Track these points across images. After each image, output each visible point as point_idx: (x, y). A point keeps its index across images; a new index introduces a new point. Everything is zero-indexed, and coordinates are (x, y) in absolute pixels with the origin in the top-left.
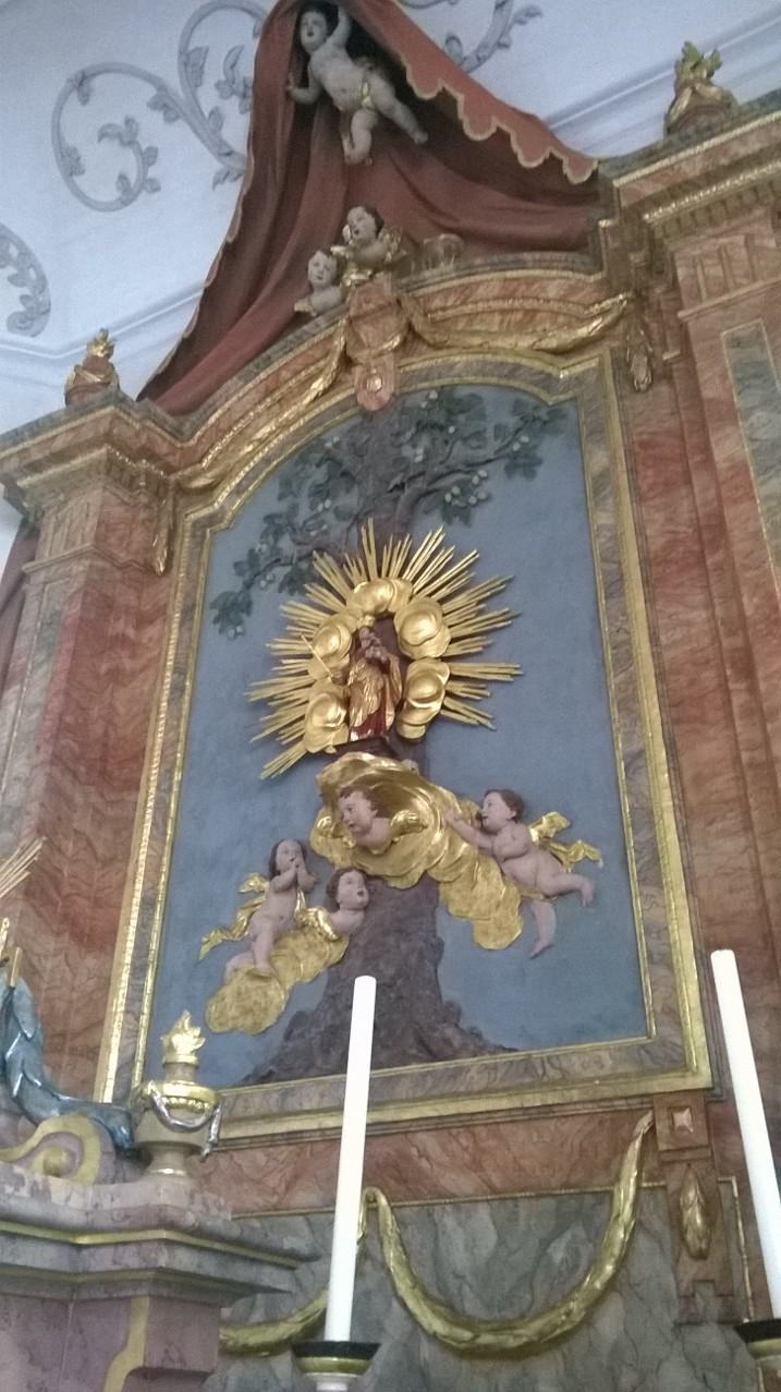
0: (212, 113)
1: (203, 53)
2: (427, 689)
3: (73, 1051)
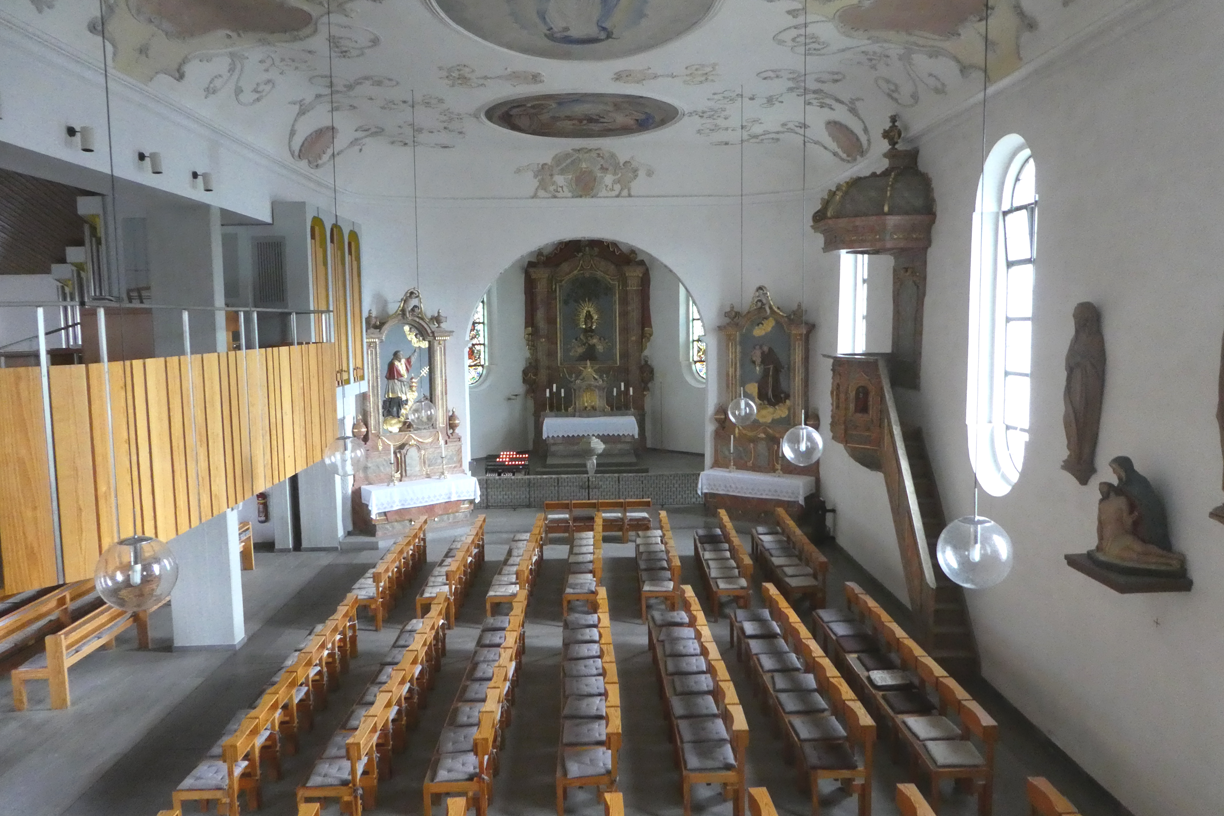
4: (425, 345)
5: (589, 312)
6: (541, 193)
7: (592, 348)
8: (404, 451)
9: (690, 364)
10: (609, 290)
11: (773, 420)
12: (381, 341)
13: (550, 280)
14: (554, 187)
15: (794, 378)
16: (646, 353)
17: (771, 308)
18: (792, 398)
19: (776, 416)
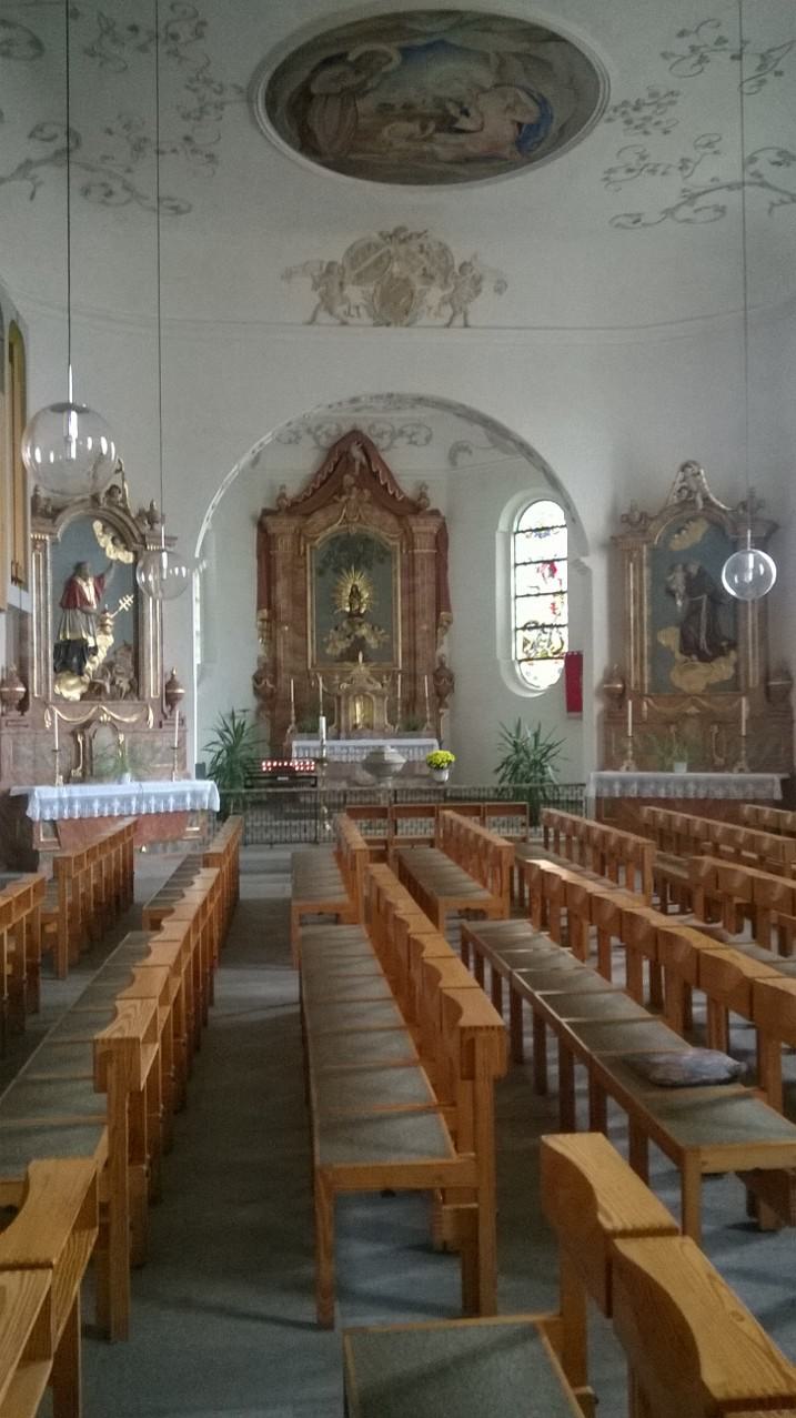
4: (127, 557)
5: (354, 586)
6: (323, 317)
8: (89, 732)
9: (512, 664)
10: (385, 555)
11: (709, 686)
12: (55, 543)
13: (299, 535)
14: (345, 307)
15: (746, 614)
16: (443, 650)
17: (706, 499)
18: (741, 647)
19: (714, 679)
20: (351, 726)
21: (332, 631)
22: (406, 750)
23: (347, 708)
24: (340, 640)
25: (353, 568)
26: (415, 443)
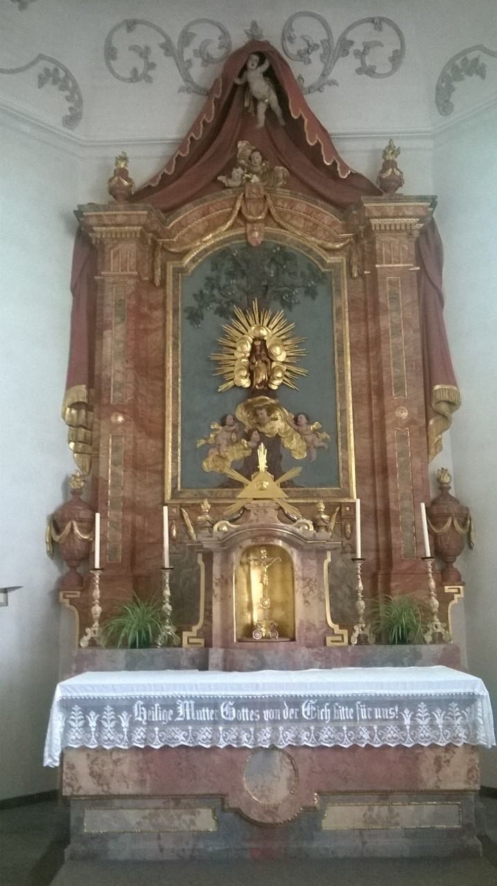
0: (187, 61)
1: (193, 35)
2: (279, 375)
3: (149, 471)
7: (248, 440)
16: (441, 461)
20: (236, 631)
21: (215, 426)
22: (391, 713)
23: (226, 581)
24: (231, 443)
25: (255, 305)
26: (371, 72)
